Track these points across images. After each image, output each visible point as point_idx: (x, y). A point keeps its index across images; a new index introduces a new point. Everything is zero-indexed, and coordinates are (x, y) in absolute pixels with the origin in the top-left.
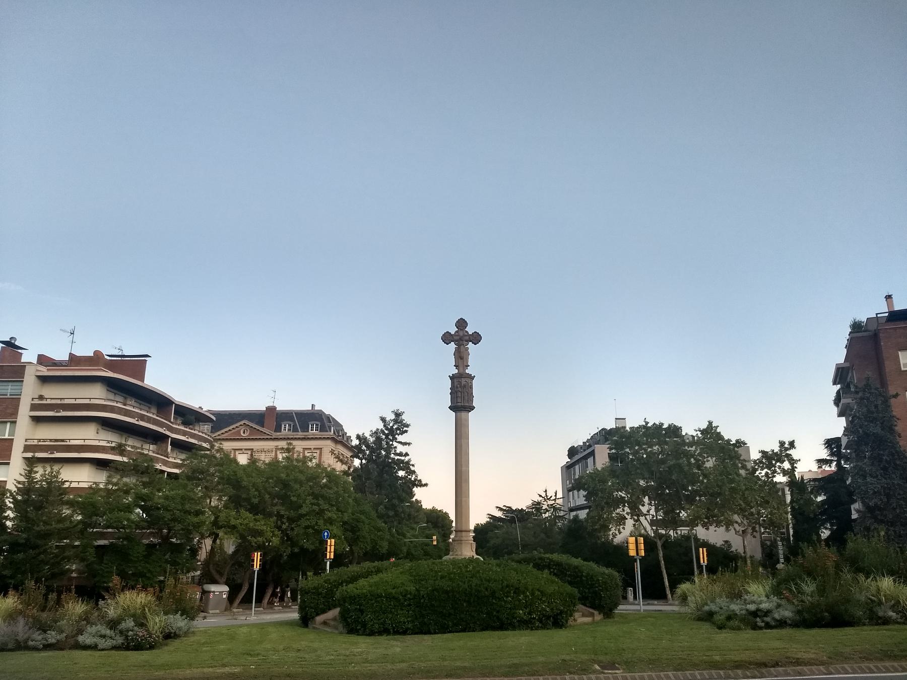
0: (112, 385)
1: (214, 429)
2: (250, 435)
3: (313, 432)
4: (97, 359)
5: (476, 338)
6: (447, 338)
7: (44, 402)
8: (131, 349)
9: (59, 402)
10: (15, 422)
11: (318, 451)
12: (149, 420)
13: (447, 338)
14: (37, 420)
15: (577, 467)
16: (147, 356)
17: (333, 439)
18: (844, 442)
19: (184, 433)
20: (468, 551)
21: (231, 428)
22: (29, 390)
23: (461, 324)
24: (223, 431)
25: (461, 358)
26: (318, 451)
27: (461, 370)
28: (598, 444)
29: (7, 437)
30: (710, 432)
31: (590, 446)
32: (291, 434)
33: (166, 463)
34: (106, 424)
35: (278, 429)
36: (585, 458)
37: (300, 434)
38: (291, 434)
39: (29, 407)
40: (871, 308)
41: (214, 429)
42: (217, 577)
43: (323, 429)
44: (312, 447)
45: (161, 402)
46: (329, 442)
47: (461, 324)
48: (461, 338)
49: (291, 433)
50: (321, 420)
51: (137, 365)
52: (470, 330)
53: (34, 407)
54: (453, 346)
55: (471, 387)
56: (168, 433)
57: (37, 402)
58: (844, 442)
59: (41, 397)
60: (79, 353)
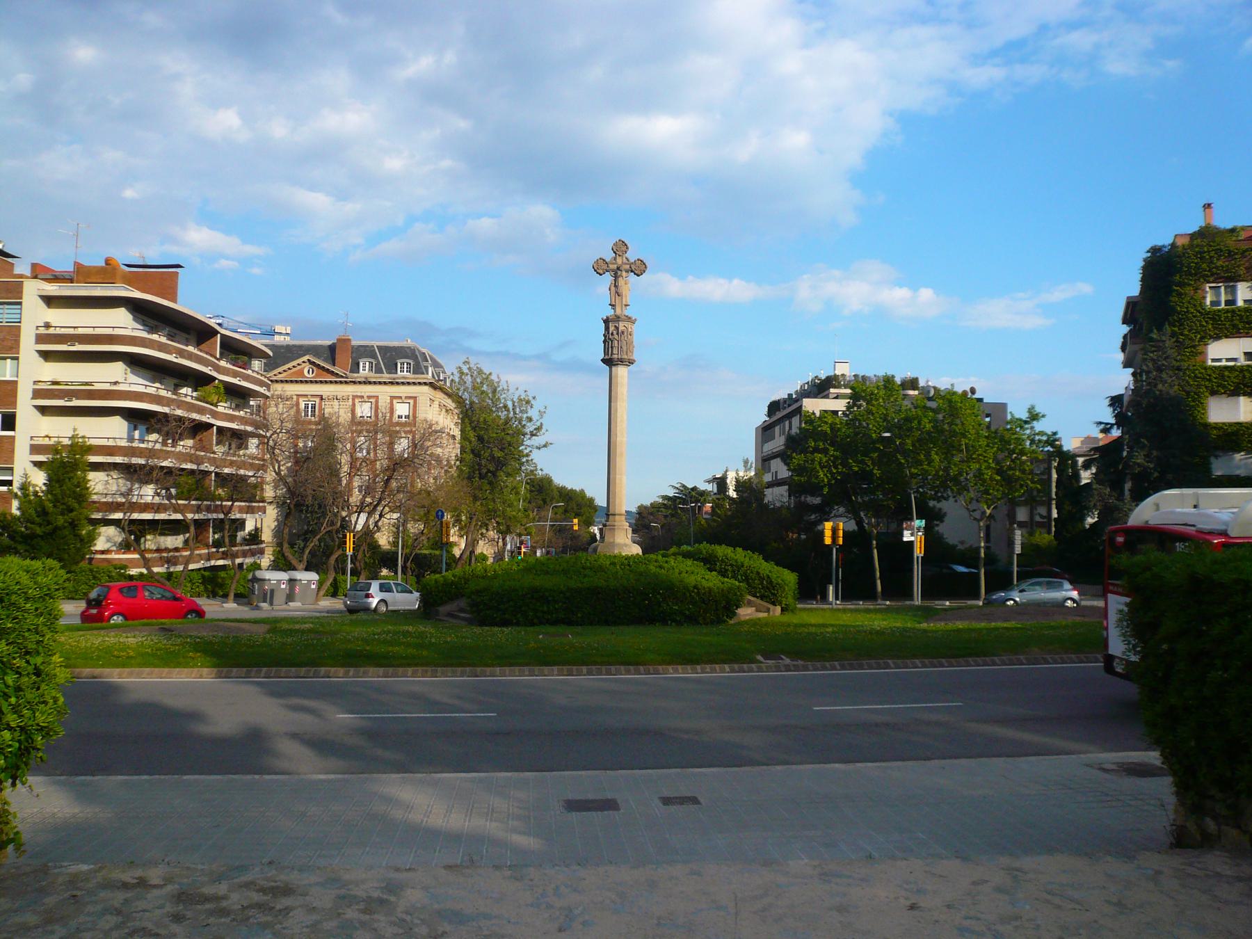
0: (139, 309)
1: (269, 367)
2: (317, 376)
3: (403, 373)
4: (108, 272)
5: (639, 269)
6: (600, 267)
7: (51, 331)
8: (154, 255)
9: (71, 331)
10: (17, 359)
11: (411, 401)
12: (190, 356)
13: (600, 267)
14: (46, 356)
15: (777, 429)
16: (178, 266)
17: (431, 385)
18: (1126, 399)
19: (235, 375)
20: (625, 544)
21: (290, 365)
22: (34, 315)
23: (620, 248)
24: (280, 369)
25: (616, 290)
26: (411, 401)
27: (618, 312)
28: (808, 397)
29: (8, 378)
30: (1126, 365)
31: (797, 400)
32: (373, 376)
33: (215, 415)
34: (136, 363)
35: (355, 368)
36: (789, 416)
37: (386, 377)
38: (373, 376)
39: (33, 339)
40: (1172, 225)
41: (269, 367)
42: (294, 562)
43: (418, 370)
44: (403, 395)
45: (200, 333)
46: (426, 388)
47: (620, 248)
48: (619, 267)
49: (372, 374)
50: (415, 358)
51: (164, 276)
52: (632, 255)
53: (40, 339)
54: (608, 278)
55: (563, 488)
56: (214, 374)
57: (42, 331)
58: (1126, 399)
59: (47, 326)
60: (86, 262)
